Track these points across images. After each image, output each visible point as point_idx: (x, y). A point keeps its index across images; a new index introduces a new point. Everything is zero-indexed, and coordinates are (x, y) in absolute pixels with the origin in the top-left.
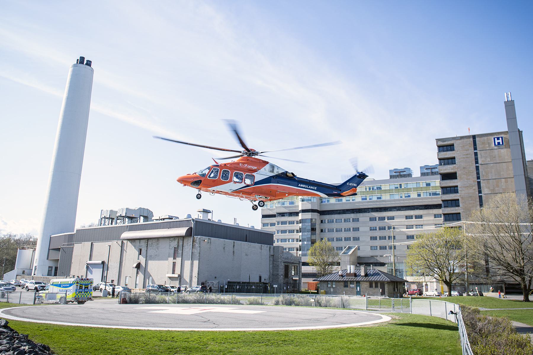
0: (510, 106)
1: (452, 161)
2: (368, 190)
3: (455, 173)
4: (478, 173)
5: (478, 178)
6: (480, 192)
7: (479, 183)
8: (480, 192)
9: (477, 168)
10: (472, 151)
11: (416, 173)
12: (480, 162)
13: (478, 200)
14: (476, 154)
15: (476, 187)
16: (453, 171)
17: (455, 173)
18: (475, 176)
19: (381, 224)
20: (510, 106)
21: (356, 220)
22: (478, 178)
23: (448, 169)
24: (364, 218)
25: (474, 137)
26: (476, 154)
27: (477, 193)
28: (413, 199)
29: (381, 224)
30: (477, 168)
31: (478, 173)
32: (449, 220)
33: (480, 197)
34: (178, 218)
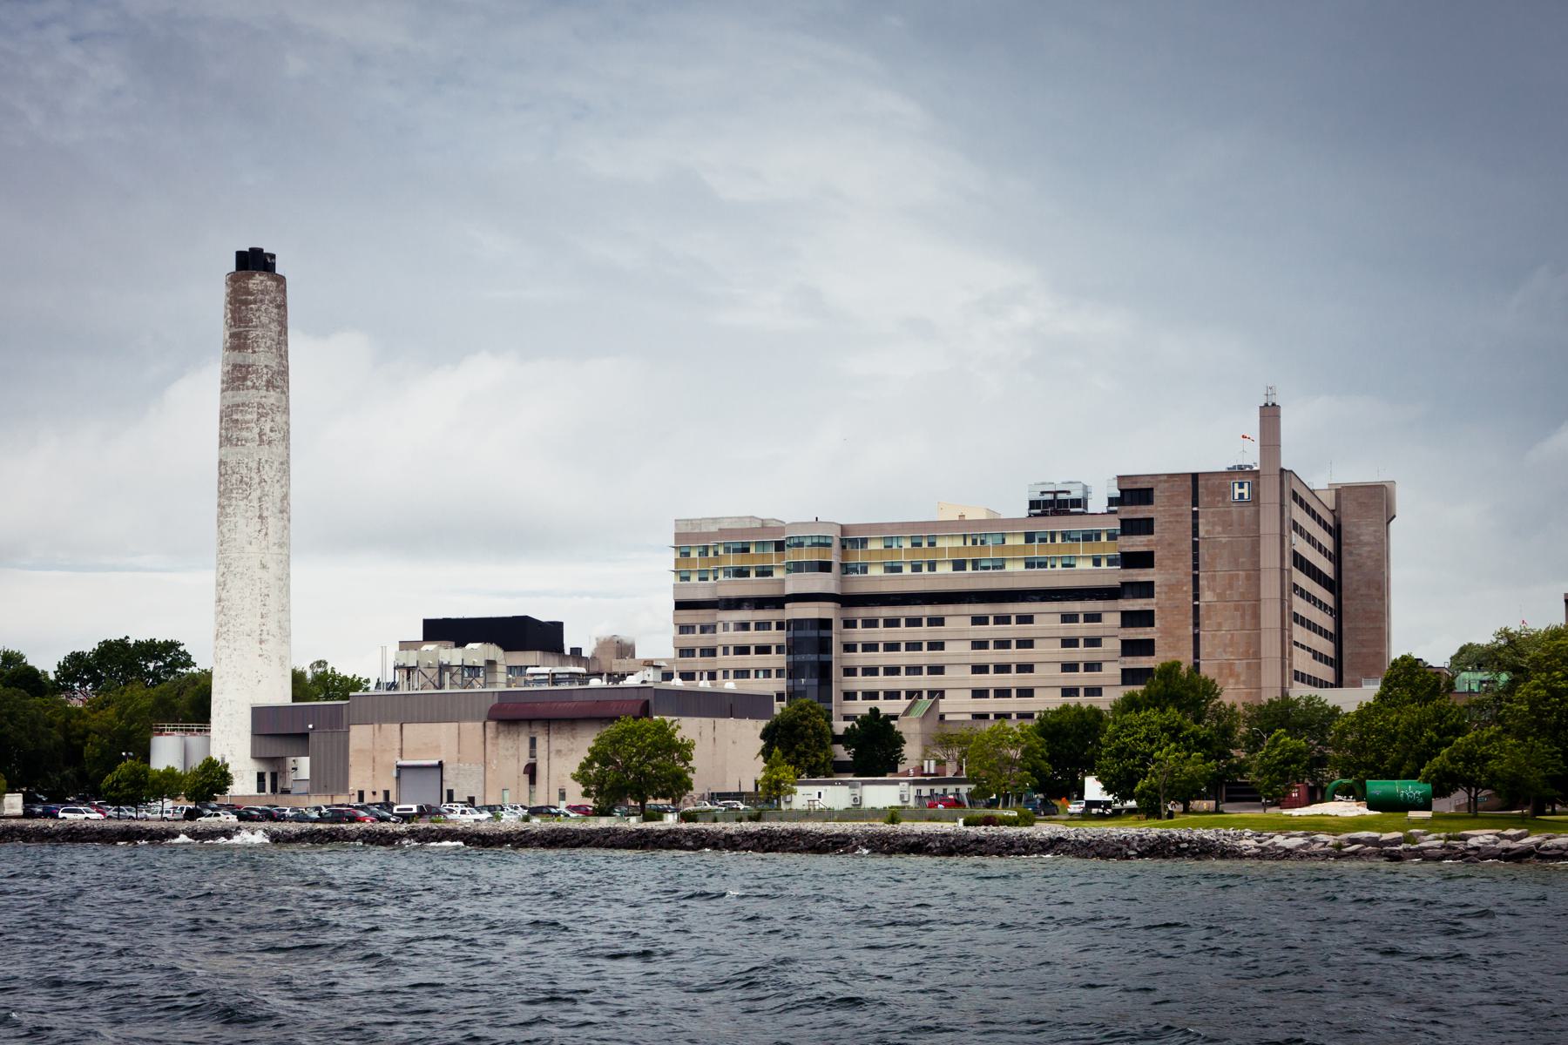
0: (1270, 414)
1: (1146, 526)
2: (969, 543)
3: (1151, 554)
4: (1196, 558)
5: (1196, 567)
6: (1196, 597)
7: (1196, 579)
8: (1196, 597)
9: (1196, 546)
10: (1188, 508)
11: (1097, 504)
12: (1202, 533)
13: (1191, 614)
14: (1195, 515)
15: (1189, 588)
16: (1145, 549)
17: (1151, 554)
18: (1190, 563)
19: (1003, 632)
20: (1270, 414)
21: (937, 621)
22: (1196, 567)
23: (1137, 543)
24: (958, 620)
25: (1195, 476)
26: (1195, 515)
27: (1191, 599)
28: (1082, 572)
29: (1003, 632)
30: (1196, 546)
31: (1196, 558)
32: (1133, 654)
33: (1196, 608)
34: (545, 636)
